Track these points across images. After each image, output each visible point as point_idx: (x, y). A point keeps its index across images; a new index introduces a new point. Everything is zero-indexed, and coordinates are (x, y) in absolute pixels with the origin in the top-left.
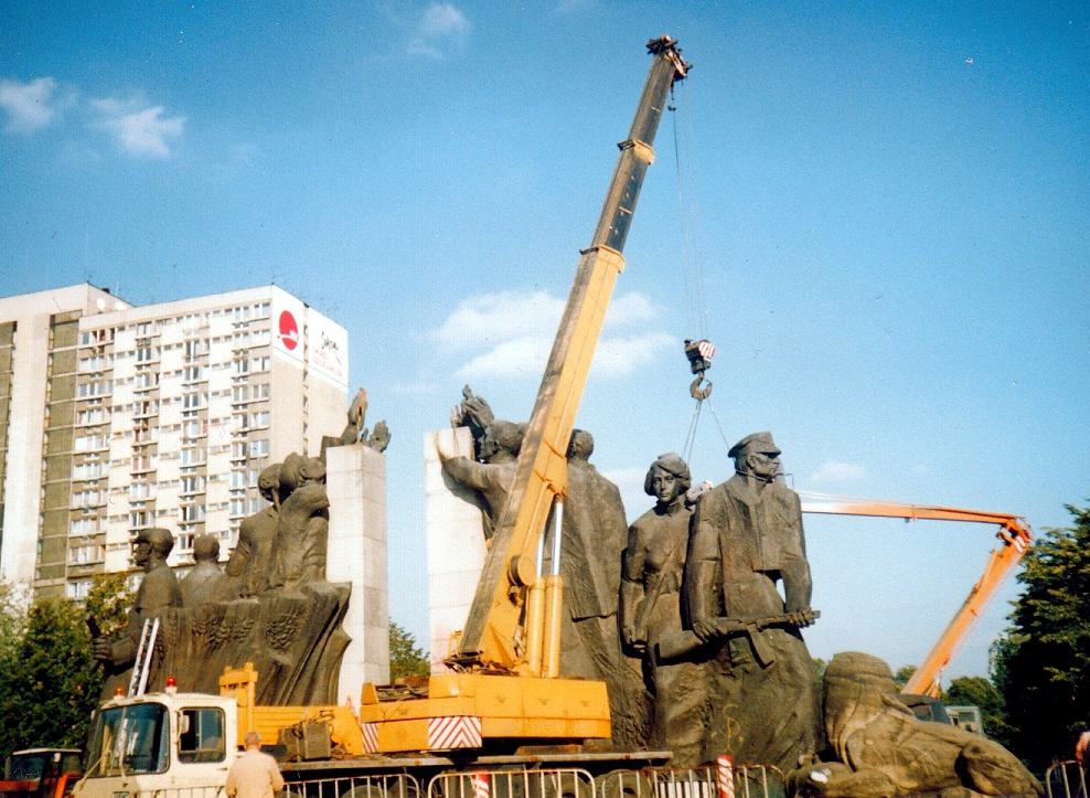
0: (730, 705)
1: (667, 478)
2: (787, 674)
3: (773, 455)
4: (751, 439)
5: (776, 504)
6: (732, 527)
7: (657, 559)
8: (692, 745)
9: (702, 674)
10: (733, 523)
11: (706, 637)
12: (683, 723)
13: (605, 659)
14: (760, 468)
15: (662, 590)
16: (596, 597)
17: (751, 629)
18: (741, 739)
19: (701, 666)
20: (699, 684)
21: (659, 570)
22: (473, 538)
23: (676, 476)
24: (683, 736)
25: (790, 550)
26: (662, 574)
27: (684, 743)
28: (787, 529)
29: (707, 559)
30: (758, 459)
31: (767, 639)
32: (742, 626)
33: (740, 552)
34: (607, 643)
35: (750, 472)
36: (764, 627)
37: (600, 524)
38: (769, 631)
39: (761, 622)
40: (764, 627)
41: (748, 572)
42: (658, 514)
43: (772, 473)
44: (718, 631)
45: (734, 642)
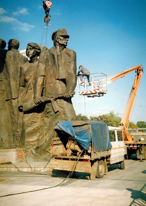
0: (46, 127)
1: (30, 49)
2: (63, 115)
3: (66, 37)
4: (59, 31)
5: (66, 55)
6: (49, 64)
7: (27, 78)
8: (34, 141)
9: (40, 117)
10: (50, 62)
11: (37, 103)
12: (32, 133)
13: (13, 113)
14: (61, 42)
15: (29, 88)
16: (11, 93)
17: (52, 100)
18: (47, 139)
19: (40, 114)
20: (39, 120)
21: (28, 82)
22: (73, 100)
23: (34, 48)
24: (31, 138)
25: (69, 72)
26: (29, 83)
27: (32, 140)
28: (69, 64)
29: (41, 76)
30: (60, 38)
31: (57, 103)
32: (49, 99)
33: (52, 72)
34: (14, 108)
35: (57, 44)
36: (56, 99)
37: (17, 69)
38: (58, 100)
39: (55, 97)
40: (56, 99)
41: (54, 80)
42: (30, 63)
43: (65, 44)
44: (41, 101)
45: (47, 105)
